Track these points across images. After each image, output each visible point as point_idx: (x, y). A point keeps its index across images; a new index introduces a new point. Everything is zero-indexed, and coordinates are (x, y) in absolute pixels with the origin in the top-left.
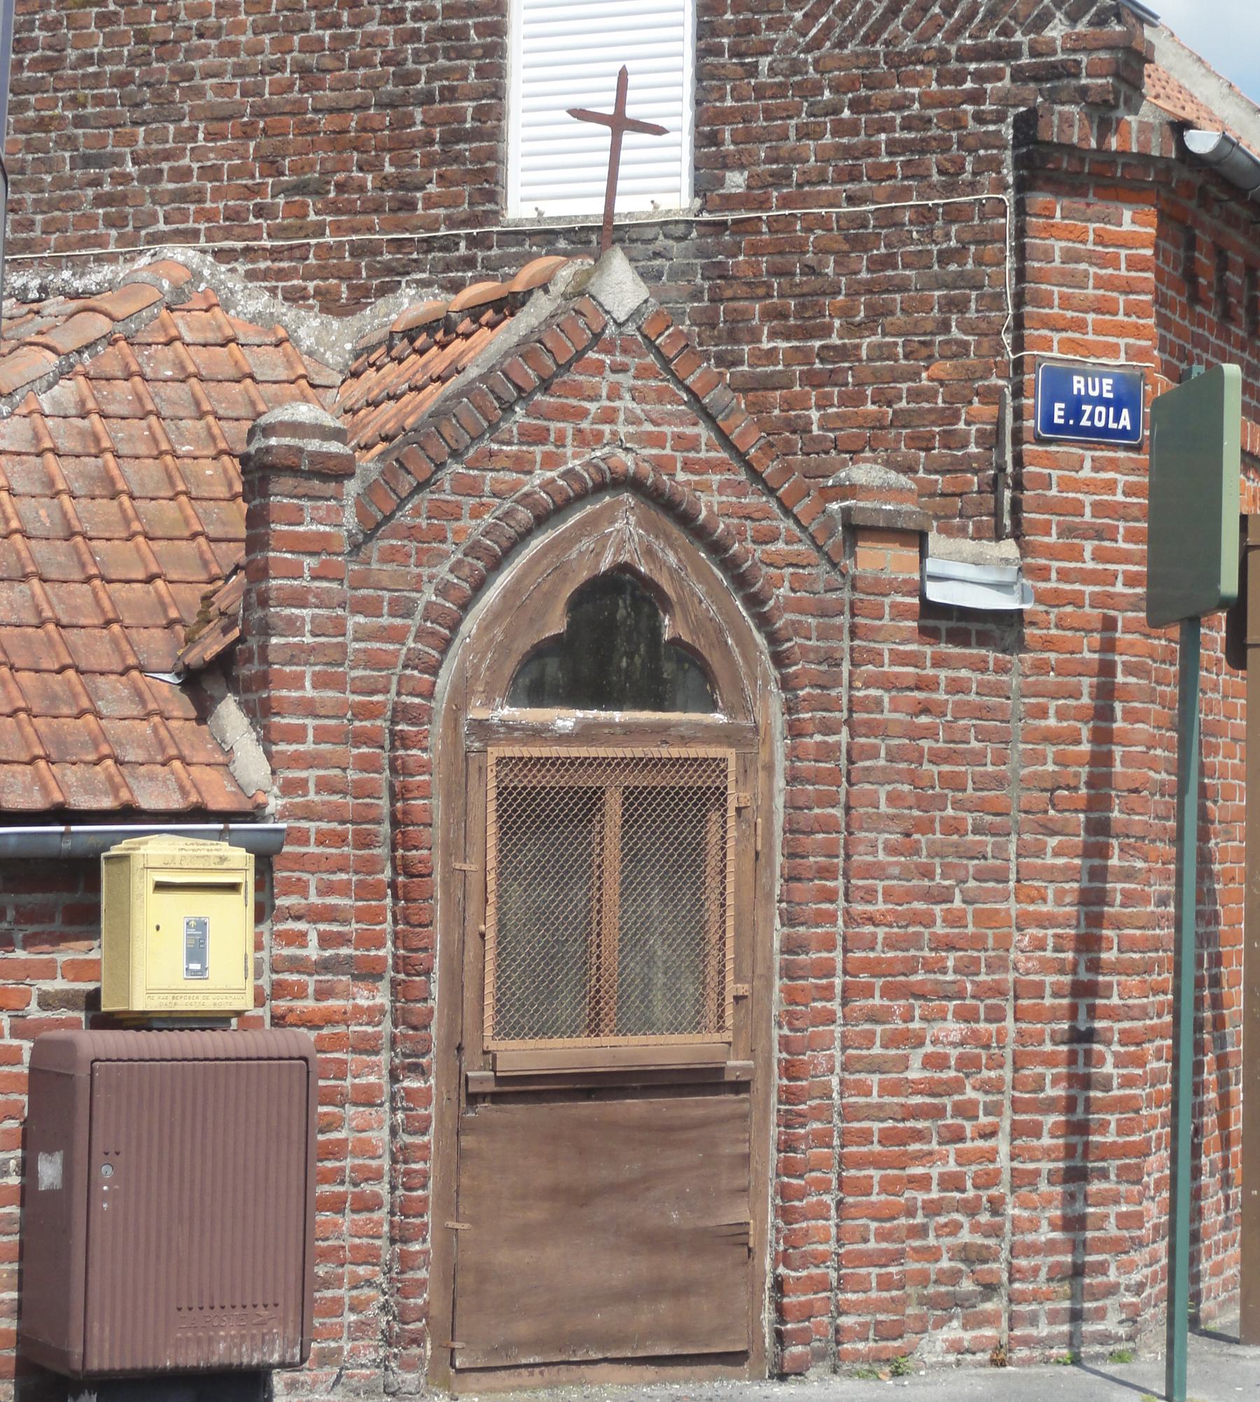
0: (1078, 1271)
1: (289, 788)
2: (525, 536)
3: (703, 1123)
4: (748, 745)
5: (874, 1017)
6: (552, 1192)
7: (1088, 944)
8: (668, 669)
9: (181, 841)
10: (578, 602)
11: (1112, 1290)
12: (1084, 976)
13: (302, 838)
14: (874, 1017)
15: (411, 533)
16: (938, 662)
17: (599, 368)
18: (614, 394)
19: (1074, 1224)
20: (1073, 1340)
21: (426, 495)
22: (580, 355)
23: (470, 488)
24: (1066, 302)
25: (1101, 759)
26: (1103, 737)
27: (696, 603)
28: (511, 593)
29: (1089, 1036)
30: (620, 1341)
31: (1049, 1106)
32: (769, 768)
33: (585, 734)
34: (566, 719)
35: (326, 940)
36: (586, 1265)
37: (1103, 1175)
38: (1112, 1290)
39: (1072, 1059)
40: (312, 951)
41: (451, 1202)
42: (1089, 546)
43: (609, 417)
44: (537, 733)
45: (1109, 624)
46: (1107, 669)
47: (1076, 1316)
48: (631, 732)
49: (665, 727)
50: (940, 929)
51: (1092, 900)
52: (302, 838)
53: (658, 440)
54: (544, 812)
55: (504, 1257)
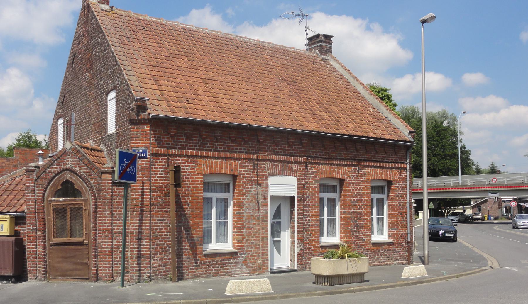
0: (139, 270)
1: (28, 209)
2: (54, 177)
3: (82, 249)
4: (86, 202)
5: (106, 236)
6: (62, 257)
7: (140, 226)
8: (76, 192)
9: (379, 171)
10: (62, 185)
11: (145, 273)
12: (140, 230)
13: (30, 214)
14: (106, 236)
15: (43, 178)
16: (117, 189)
17: (66, 156)
18: (68, 158)
19: (139, 264)
20: (139, 279)
21: (45, 173)
22: (63, 154)
23: (50, 172)
24: (136, 140)
25: (142, 201)
26: (142, 198)
27: (78, 183)
28: (53, 184)
29: (141, 239)
30: (71, 276)
31: (135, 248)
32: (90, 204)
33: (64, 201)
34: (61, 199)
35: (33, 226)
36: (66, 266)
37: (144, 257)
38: (145, 273)
39: (138, 242)
40: (31, 228)
41: (49, 258)
42: (140, 173)
43: (68, 161)
44: (58, 201)
45: (143, 183)
46: (143, 189)
47: (139, 276)
48: (70, 200)
49: (75, 200)
50: (118, 224)
51: (141, 220)
52: (30, 214)
53: (75, 164)
54: (60, 211)
55: (56, 265)
